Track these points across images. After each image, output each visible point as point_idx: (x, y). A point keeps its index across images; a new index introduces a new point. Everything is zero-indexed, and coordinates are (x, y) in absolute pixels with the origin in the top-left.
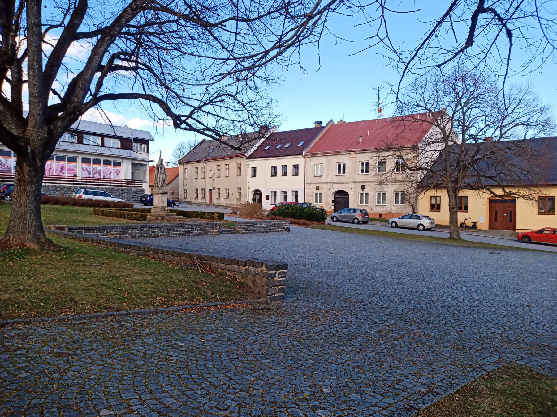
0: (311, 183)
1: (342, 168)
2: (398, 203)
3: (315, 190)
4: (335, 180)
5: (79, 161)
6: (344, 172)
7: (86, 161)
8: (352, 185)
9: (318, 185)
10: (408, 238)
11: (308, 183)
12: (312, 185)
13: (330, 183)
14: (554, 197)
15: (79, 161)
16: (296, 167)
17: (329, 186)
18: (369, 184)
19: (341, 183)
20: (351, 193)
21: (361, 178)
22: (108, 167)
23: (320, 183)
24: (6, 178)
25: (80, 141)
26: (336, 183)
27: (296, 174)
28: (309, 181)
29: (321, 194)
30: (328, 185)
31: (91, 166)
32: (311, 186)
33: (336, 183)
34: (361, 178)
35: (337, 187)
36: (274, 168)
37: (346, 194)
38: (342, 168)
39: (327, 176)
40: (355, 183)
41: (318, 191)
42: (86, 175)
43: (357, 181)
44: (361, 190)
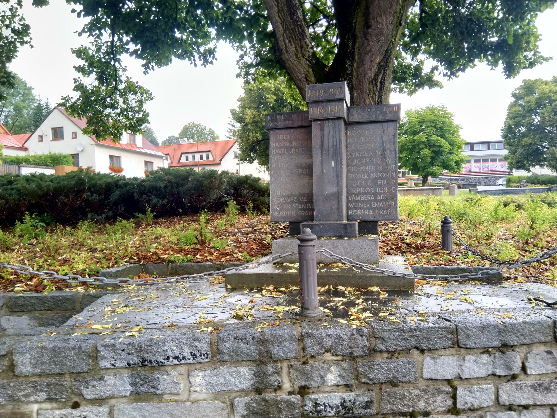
5: (472, 161)
7: (477, 161)
15: (472, 161)
22: (494, 163)
25: (472, 149)
31: (481, 164)
42: (478, 170)
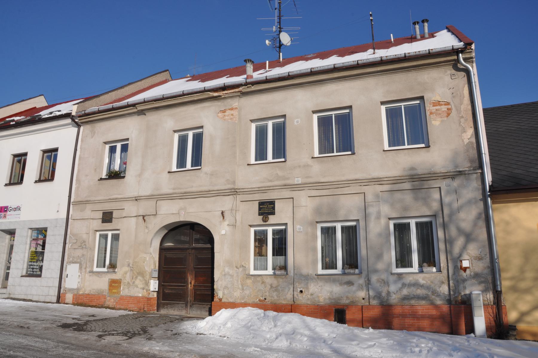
0: (87, 202)
1: (192, 150)
2: (333, 266)
3: (97, 224)
4: (166, 189)
6: (197, 161)
8: (227, 203)
9: (108, 207)
10: (17, 345)
11: (79, 203)
12: (89, 207)
13: (149, 197)
14: (47, 228)
16: (51, 154)
17: (144, 207)
18: (287, 194)
19: (184, 196)
20: (221, 233)
21: (255, 176)
23: (116, 200)
24: (353, 234)
26: (170, 197)
27: (48, 175)
28: (83, 196)
29: (116, 238)
30: (143, 203)
32: (88, 212)
33: (170, 197)
34: (255, 176)
35: (173, 212)
36: (20, 159)
37: (207, 237)
38: (192, 150)
39: (140, 175)
40: (234, 192)
41: (107, 226)
43: (240, 184)
44: (259, 220)
